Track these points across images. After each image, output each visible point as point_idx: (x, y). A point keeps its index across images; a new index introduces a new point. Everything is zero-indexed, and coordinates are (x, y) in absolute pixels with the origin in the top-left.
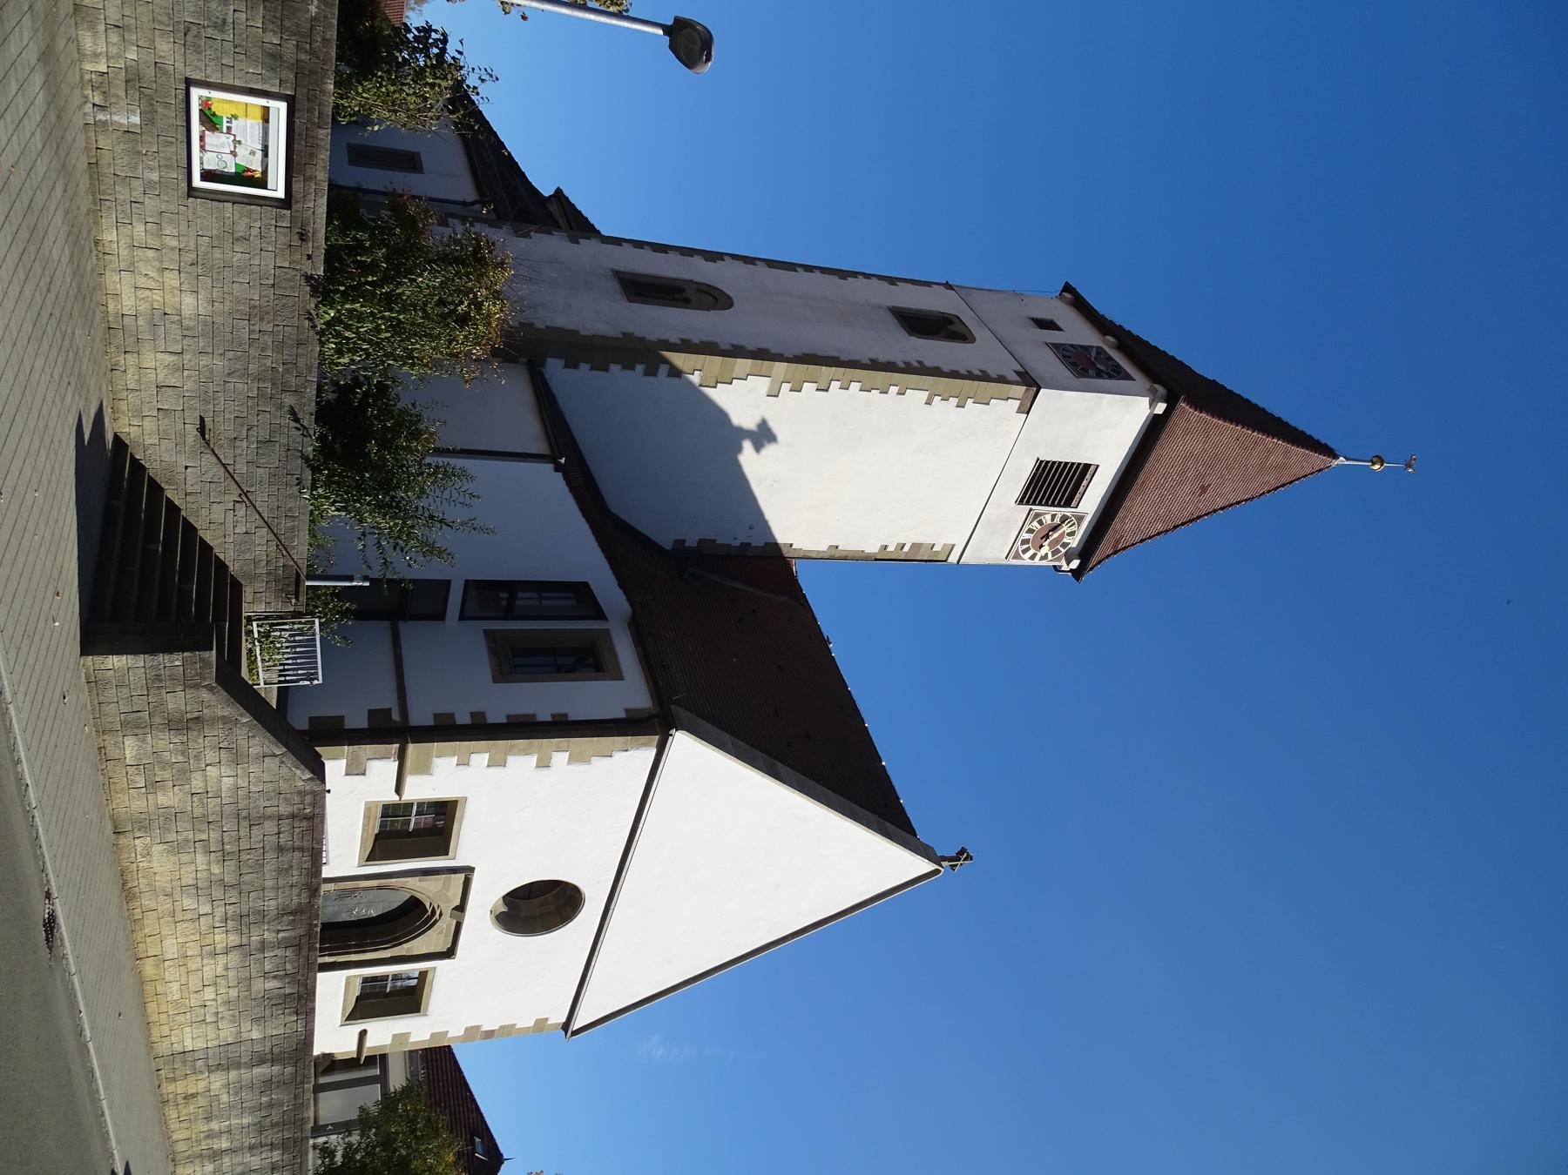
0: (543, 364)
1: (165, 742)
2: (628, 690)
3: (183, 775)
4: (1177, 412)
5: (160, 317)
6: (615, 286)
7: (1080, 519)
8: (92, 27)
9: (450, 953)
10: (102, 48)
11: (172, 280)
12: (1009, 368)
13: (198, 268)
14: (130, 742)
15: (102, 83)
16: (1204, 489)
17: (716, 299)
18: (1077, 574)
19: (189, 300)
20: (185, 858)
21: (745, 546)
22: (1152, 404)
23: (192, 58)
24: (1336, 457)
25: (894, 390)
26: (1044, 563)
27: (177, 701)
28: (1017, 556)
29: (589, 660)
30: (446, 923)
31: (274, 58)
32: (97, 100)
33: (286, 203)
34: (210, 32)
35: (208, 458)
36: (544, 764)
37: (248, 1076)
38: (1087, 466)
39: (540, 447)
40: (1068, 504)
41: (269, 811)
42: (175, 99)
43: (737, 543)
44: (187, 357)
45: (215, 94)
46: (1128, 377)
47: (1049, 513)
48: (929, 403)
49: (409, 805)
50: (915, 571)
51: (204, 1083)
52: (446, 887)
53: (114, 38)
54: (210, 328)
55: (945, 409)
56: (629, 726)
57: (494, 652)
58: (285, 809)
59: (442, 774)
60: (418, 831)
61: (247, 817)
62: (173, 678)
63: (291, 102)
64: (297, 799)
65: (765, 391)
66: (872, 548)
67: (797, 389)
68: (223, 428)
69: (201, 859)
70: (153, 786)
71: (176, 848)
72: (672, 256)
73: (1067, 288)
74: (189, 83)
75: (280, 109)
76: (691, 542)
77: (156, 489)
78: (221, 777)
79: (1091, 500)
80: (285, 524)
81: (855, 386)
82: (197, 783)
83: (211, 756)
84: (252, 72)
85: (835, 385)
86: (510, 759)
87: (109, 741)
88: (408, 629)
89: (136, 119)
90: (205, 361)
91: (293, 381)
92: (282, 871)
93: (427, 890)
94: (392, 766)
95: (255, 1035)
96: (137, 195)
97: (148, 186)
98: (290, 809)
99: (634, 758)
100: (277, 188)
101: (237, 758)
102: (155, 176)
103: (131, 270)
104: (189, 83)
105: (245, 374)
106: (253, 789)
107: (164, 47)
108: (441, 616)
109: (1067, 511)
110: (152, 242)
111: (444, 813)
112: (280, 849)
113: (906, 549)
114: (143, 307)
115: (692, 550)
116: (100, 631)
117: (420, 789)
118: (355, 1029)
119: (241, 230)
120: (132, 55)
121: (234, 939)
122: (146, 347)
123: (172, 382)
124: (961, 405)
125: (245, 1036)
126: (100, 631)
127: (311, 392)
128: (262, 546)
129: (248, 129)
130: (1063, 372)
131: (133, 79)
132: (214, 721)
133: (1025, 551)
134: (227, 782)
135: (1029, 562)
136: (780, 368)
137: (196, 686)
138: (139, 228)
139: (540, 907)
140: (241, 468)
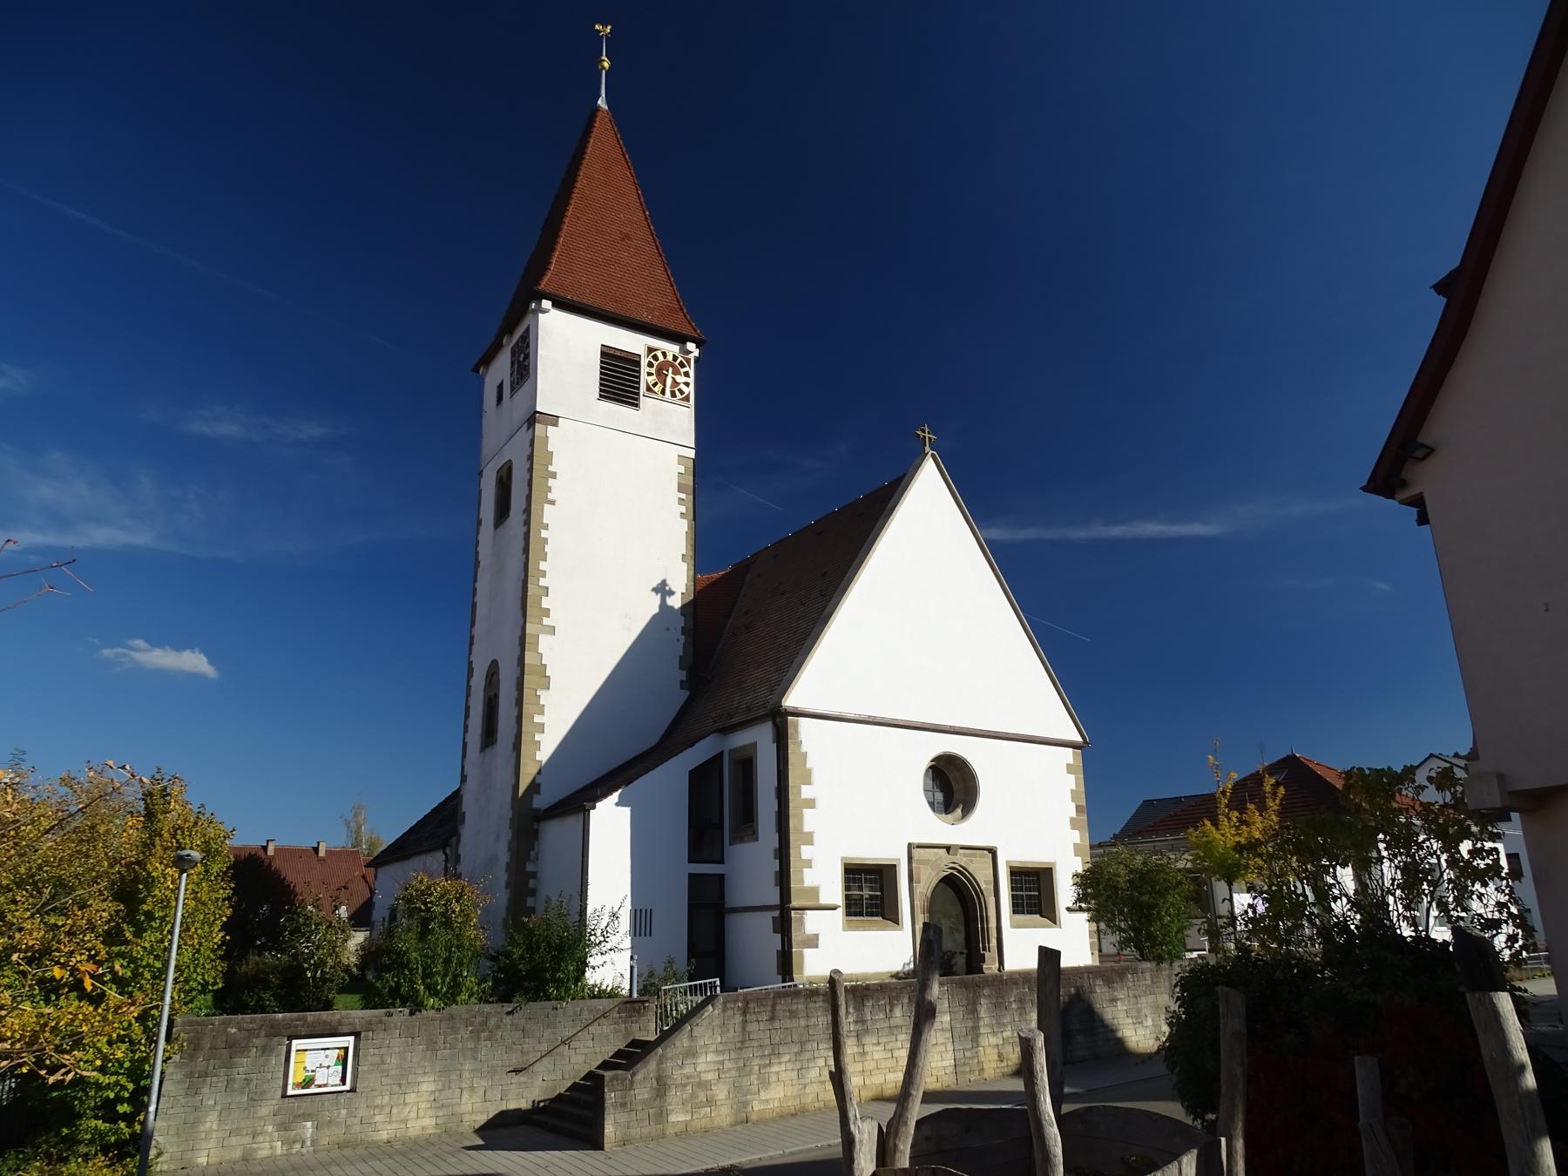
1: (674, 1096)
2: (760, 736)
3: (704, 1085)
4: (550, 290)
5: (437, 1103)
6: (488, 750)
7: (650, 350)
8: (255, 1150)
9: (993, 852)
10: (267, 1145)
11: (411, 1098)
12: (524, 433)
13: (403, 1082)
14: (672, 1118)
15: (289, 1143)
16: (626, 237)
17: (493, 672)
19: (425, 1087)
20: (773, 1078)
21: (684, 631)
22: (545, 311)
23: (269, 1096)
24: (597, 109)
26: (692, 373)
27: (642, 1092)
28: (687, 399)
29: (746, 764)
30: (961, 859)
31: (265, 1050)
32: (298, 1146)
33: (357, 1035)
34: (252, 1087)
35: (535, 1067)
36: (811, 803)
37: (987, 1021)
38: (603, 354)
39: (581, 816)
40: (638, 364)
41: (738, 1028)
42: (295, 1103)
43: (682, 638)
45: (291, 1081)
46: (527, 330)
47: (646, 378)
48: (552, 503)
49: (847, 898)
51: (989, 1051)
52: (926, 862)
53: (260, 1138)
54: (445, 1072)
55: (557, 488)
56: (782, 739)
57: (742, 840)
58: (738, 1018)
59: (819, 874)
60: (870, 890)
62: (624, 1097)
63: (291, 1038)
64: (730, 1013)
65: (549, 637)
67: (547, 612)
68: (515, 1060)
69: (775, 1069)
70: (710, 1102)
71: (765, 1083)
72: (471, 703)
74: (284, 1096)
75: (297, 1044)
76: (683, 675)
77: (559, 1098)
78: (706, 1063)
80: (585, 1014)
82: (711, 1076)
83: (688, 1070)
84: (275, 1061)
85: (543, 582)
86: (806, 829)
87: (670, 1131)
88: (733, 900)
89: (309, 1124)
90: (466, 1075)
91: (479, 1019)
92: (793, 1014)
93: (928, 880)
94: (810, 916)
95: (947, 1018)
96: (357, 1121)
97: (350, 1114)
99: (807, 734)
100: (349, 1041)
101: (692, 1053)
102: (344, 1112)
103: (405, 1121)
104: (284, 1096)
105: (475, 1050)
107: (264, 1111)
108: (721, 877)
109: (644, 362)
110: (387, 1110)
111: (855, 873)
112: (772, 1018)
114: (430, 1113)
115: (689, 675)
116: (591, 1139)
117: (833, 890)
118: (1063, 914)
119: (377, 1059)
120: (270, 1128)
122: (457, 1109)
124: (554, 475)
125: (946, 1025)
126: (591, 1139)
127: (487, 1008)
128: (605, 1028)
129: (311, 1061)
130: (522, 393)
131: (284, 1127)
133: (682, 392)
134: (711, 1057)
136: (530, 629)
137: (632, 1082)
138: (378, 1118)
139: (952, 785)
140: (544, 1047)
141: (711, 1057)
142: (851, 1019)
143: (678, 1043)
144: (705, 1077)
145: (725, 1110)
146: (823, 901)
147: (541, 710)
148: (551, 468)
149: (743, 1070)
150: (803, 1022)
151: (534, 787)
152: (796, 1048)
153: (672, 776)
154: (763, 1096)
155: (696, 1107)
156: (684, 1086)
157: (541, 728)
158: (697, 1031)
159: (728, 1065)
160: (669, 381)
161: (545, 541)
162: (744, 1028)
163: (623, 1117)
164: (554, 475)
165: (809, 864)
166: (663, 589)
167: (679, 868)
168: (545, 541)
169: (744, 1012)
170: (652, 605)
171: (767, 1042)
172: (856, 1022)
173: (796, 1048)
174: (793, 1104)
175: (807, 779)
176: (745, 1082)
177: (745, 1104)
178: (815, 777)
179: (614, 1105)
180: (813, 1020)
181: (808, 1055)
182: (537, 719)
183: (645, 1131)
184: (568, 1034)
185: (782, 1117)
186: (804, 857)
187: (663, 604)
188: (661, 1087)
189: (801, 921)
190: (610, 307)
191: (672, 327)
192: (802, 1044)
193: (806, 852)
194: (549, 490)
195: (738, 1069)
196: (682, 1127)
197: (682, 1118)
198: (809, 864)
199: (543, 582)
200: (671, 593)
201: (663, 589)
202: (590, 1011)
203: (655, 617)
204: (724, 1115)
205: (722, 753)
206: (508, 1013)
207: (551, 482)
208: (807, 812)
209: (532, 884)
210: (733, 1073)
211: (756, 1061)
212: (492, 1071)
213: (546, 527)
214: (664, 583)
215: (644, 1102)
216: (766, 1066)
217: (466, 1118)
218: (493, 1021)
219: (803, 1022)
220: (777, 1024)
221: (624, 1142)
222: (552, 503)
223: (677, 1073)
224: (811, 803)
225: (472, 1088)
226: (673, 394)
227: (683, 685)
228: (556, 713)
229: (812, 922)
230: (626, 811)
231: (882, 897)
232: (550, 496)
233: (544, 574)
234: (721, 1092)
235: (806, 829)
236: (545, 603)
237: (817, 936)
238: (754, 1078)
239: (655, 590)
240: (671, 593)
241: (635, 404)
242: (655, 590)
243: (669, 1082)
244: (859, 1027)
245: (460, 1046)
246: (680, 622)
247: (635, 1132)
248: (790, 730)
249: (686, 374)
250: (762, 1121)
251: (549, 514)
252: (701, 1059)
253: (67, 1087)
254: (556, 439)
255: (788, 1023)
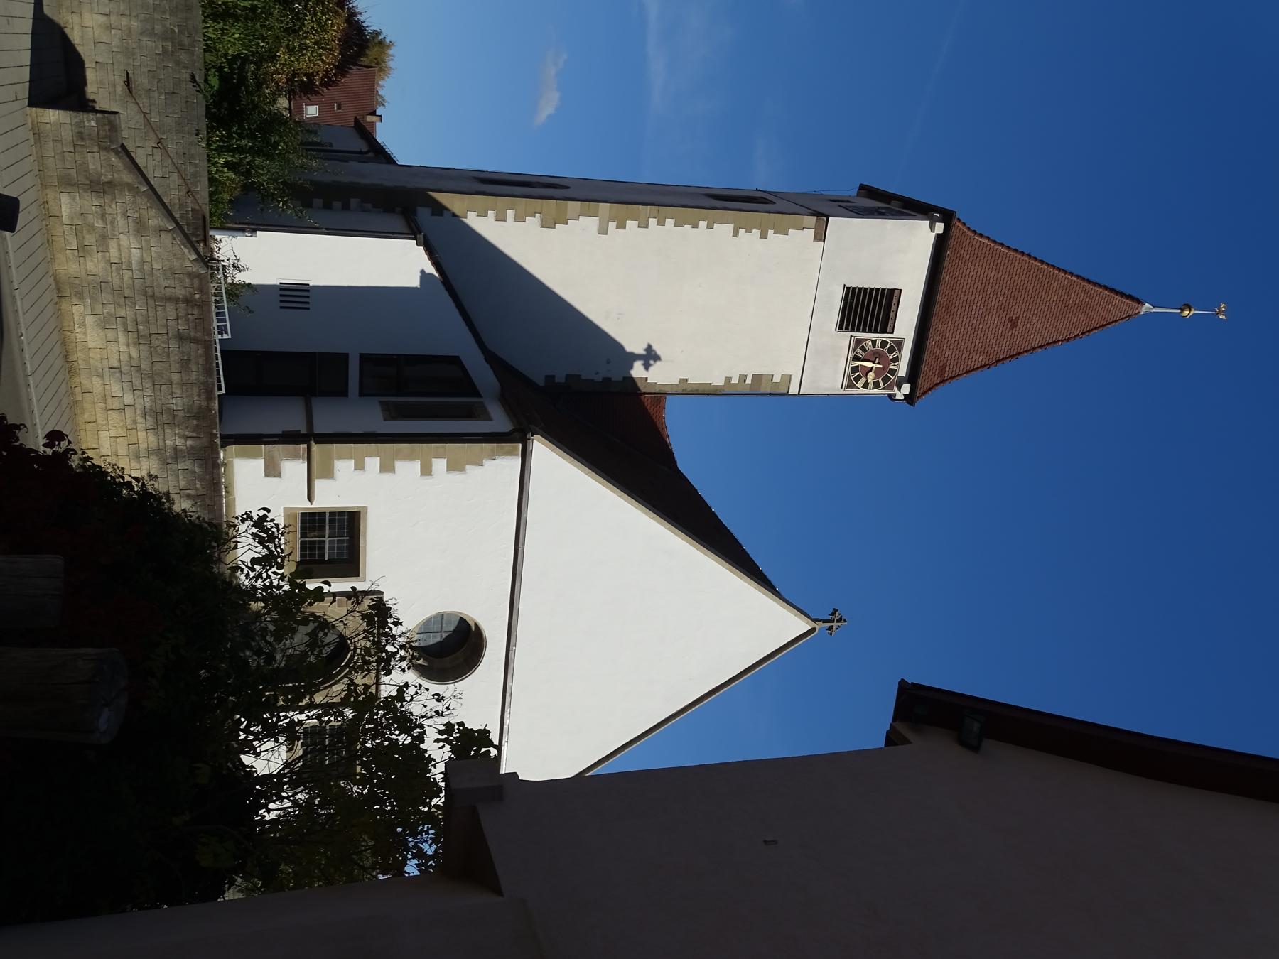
0: (415, 213)
1: (91, 203)
2: (499, 421)
7: (899, 343)
14: (65, 198)
16: (1014, 323)
18: (909, 399)
20: (111, 335)
22: (932, 227)
25: (703, 224)
28: (851, 386)
36: (426, 471)
38: (893, 290)
40: (884, 331)
41: (169, 291)
43: (599, 378)
44: (113, 18)
48: (735, 234)
50: (759, 398)
58: (180, 293)
61: (153, 296)
65: (595, 229)
66: (718, 381)
67: (621, 226)
68: (141, 80)
69: (121, 337)
70: (83, 249)
71: (105, 322)
73: (862, 187)
78: (129, 247)
79: (906, 324)
81: (670, 222)
82: (113, 251)
83: (121, 223)
85: (653, 222)
86: (399, 465)
87: (51, 194)
90: (124, 21)
91: (186, 41)
92: (185, 365)
98: (183, 292)
99: (505, 467)
101: (141, 229)
105: (152, 34)
106: (156, 266)
108: (346, 395)
109: (885, 336)
112: (180, 337)
113: (749, 381)
116: (41, 96)
121: (152, 441)
123: (104, 39)
124: (764, 236)
126: (41, 96)
127: (199, 50)
132: (123, 185)
133: (857, 379)
135: (864, 391)
136: (604, 207)
137: (107, 149)
140: (155, 118)
141: (136, 253)
142: (179, 442)
143: (153, 212)
144: (113, 245)
145: (73, 268)
146: (319, 484)
147: (519, 218)
148: (771, 232)
149: (120, 295)
150: (175, 377)
151: (439, 209)
152: (145, 366)
153: (450, 337)
154: (90, 320)
155: (78, 231)
156: (103, 217)
157: (501, 218)
158: (166, 239)
159: (127, 275)
160: (869, 365)
161: (696, 226)
162: (169, 299)
163: (67, 134)
164: (764, 236)
165: (360, 467)
166: (650, 356)
167: (352, 342)
168: (696, 226)
169: (188, 301)
170: (634, 346)
171: (154, 330)
172: (175, 448)
173: (145, 366)
174: (79, 358)
175: (454, 466)
176: (106, 297)
177: (80, 295)
178: (456, 477)
179: (80, 124)
180: (177, 391)
181: (137, 382)
182: (510, 214)
183: (50, 163)
184: (169, 150)
185: (64, 343)
186: (367, 460)
187: (634, 357)
188: (100, 187)
189: (295, 456)
190: (941, 299)
191: (924, 367)
192: (151, 375)
193: (373, 463)
194: (749, 231)
195: (122, 289)
196: (54, 211)
197: (65, 211)
198: (360, 467)
199: (653, 222)
200: (647, 366)
201: (650, 356)
202: (195, 175)
203: (620, 347)
204: (68, 266)
205: (480, 396)
206: (193, 77)
207: (756, 232)
208: (417, 465)
209: (337, 204)
210: (117, 282)
211: (130, 314)
212: (128, 53)
213: (710, 227)
214: (657, 358)
215: (85, 163)
216: (125, 325)
217: (76, 18)
218: (184, 57)
219: (175, 377)
220: (173, 343)
221: (37, 134)
222: (735, 234)
223: (115, 209)
224: (426, 471)
225: (110, 28)
226: (854, 369)
227: (550, 378)
228: (512, 234)
229: (294, 470)
230: (415, 282)
231: (323, 561)
232: (742, 231)
233: (661, 223)
234: (94, 264)
235: (399, 465)
236: (631, 225)
237: (279, 475)
238: (110, 308)
239: (649, 348)
240: (647, 366)
241: (842, 327)
242: (649, 348)
243: (108, 197)
244: (169, 452)
245: (157, 16)
246: (617, 377)
247: (49, 150)
248: (507, 446)
249: (876, 385)
250: (59, 315)
251: (724, 230)
252: (134, 242)
253: (177, 223)
254: (802, 237)
255: (174, 358)
